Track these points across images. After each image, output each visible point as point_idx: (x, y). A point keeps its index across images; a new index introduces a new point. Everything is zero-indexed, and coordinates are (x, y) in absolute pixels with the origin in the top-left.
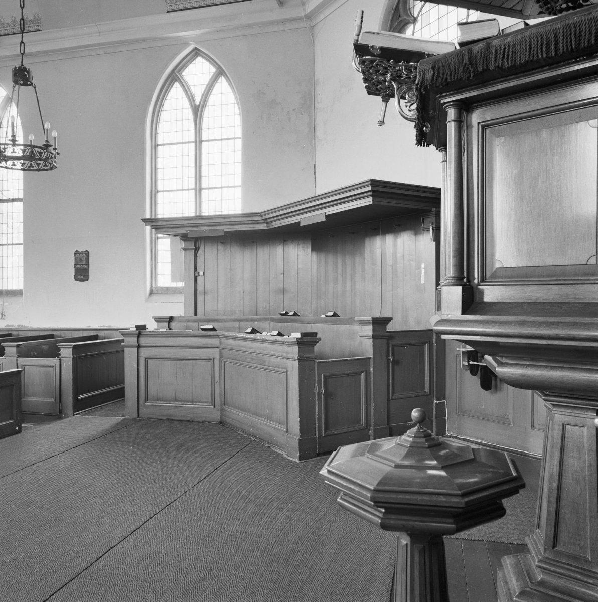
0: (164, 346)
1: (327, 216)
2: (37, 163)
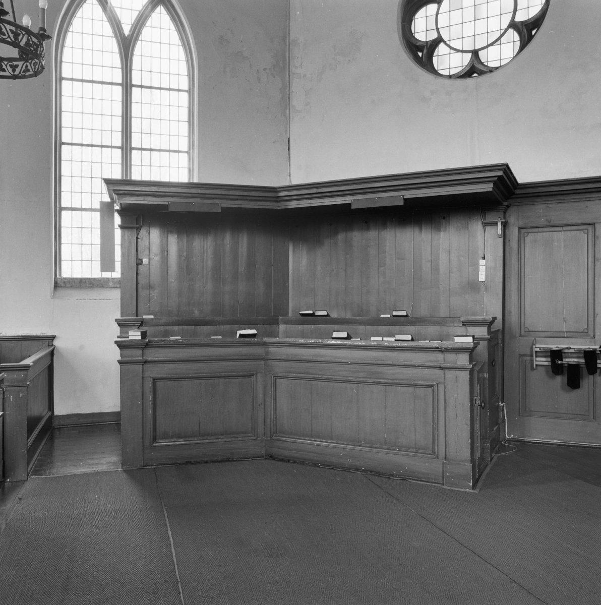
0: (180, 361)
1: (405, 200)
2: (11, 66)
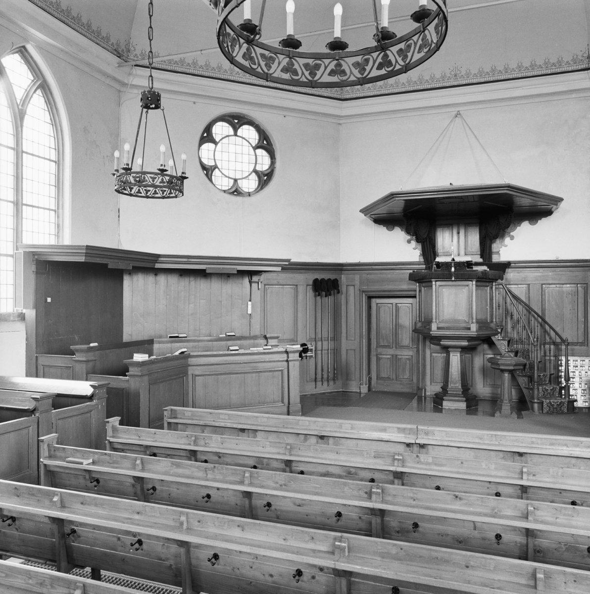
2: (162, 191)
